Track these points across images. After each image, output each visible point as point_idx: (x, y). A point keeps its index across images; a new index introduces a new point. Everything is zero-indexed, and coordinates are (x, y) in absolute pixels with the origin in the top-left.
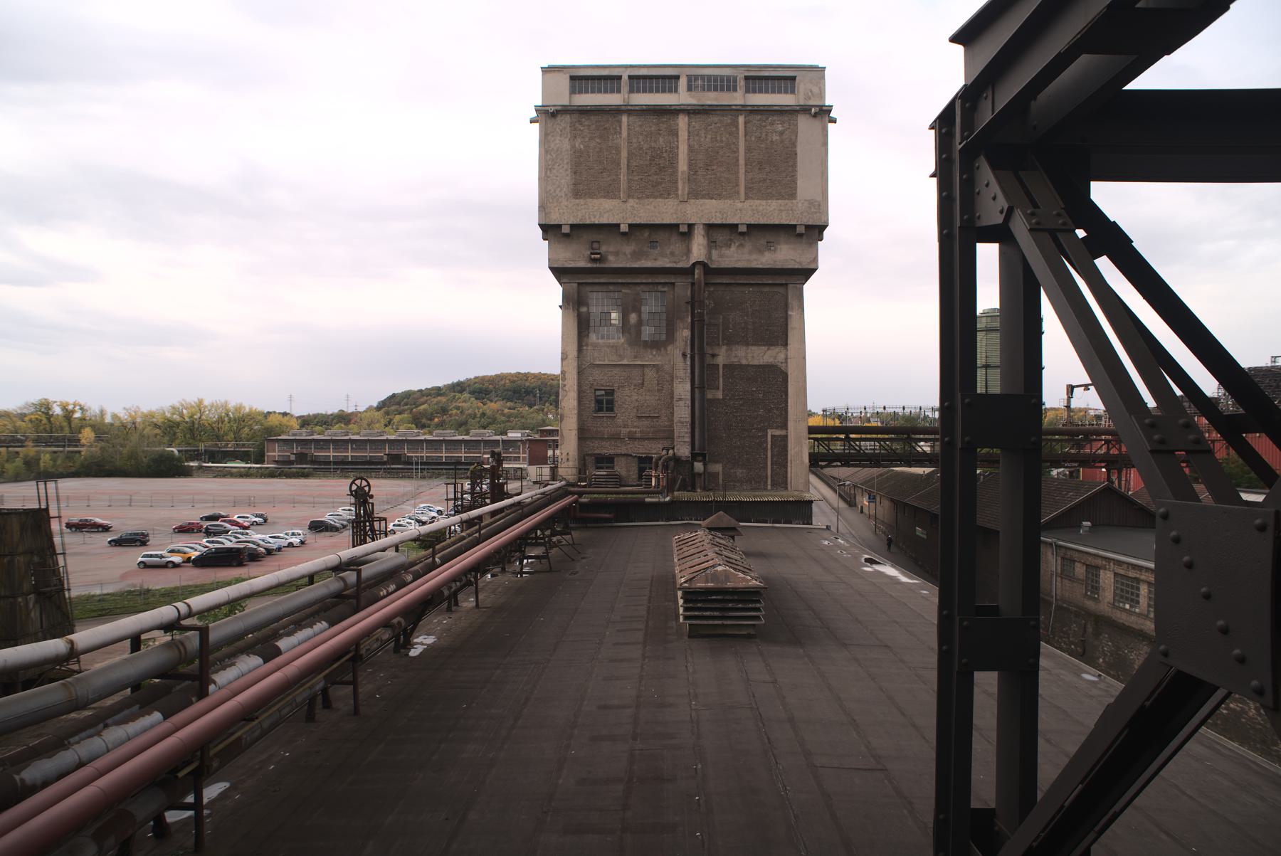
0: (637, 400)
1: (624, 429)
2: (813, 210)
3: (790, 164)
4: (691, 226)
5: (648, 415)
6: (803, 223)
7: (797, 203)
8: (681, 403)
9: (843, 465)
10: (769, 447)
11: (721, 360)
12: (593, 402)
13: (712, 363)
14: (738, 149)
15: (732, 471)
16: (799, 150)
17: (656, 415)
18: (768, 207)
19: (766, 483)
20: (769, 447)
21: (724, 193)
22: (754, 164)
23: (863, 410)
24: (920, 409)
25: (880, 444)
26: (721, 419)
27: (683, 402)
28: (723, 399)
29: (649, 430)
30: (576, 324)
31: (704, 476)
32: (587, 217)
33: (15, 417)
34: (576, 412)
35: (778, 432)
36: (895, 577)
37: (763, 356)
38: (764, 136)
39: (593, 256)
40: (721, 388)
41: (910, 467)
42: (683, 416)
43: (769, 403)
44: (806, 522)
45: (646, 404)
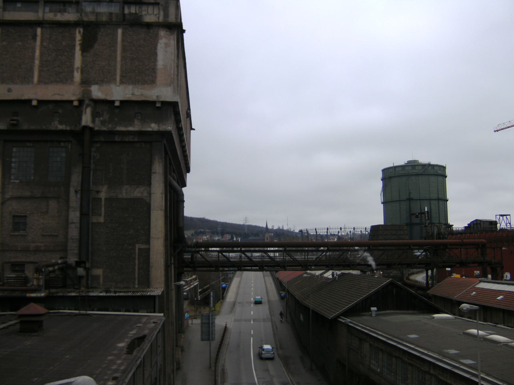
5: (49, 234)
8: (73, 226)
10: (137, 257)
11: (103, 195)
17: (56, 234)
20: (137, 257)
21: (106, 80)
23: (339, 230)
31: (87, 280)
35: (143, 246)
36: (437, 361)
39: (11, 122)
40: (103, 214)
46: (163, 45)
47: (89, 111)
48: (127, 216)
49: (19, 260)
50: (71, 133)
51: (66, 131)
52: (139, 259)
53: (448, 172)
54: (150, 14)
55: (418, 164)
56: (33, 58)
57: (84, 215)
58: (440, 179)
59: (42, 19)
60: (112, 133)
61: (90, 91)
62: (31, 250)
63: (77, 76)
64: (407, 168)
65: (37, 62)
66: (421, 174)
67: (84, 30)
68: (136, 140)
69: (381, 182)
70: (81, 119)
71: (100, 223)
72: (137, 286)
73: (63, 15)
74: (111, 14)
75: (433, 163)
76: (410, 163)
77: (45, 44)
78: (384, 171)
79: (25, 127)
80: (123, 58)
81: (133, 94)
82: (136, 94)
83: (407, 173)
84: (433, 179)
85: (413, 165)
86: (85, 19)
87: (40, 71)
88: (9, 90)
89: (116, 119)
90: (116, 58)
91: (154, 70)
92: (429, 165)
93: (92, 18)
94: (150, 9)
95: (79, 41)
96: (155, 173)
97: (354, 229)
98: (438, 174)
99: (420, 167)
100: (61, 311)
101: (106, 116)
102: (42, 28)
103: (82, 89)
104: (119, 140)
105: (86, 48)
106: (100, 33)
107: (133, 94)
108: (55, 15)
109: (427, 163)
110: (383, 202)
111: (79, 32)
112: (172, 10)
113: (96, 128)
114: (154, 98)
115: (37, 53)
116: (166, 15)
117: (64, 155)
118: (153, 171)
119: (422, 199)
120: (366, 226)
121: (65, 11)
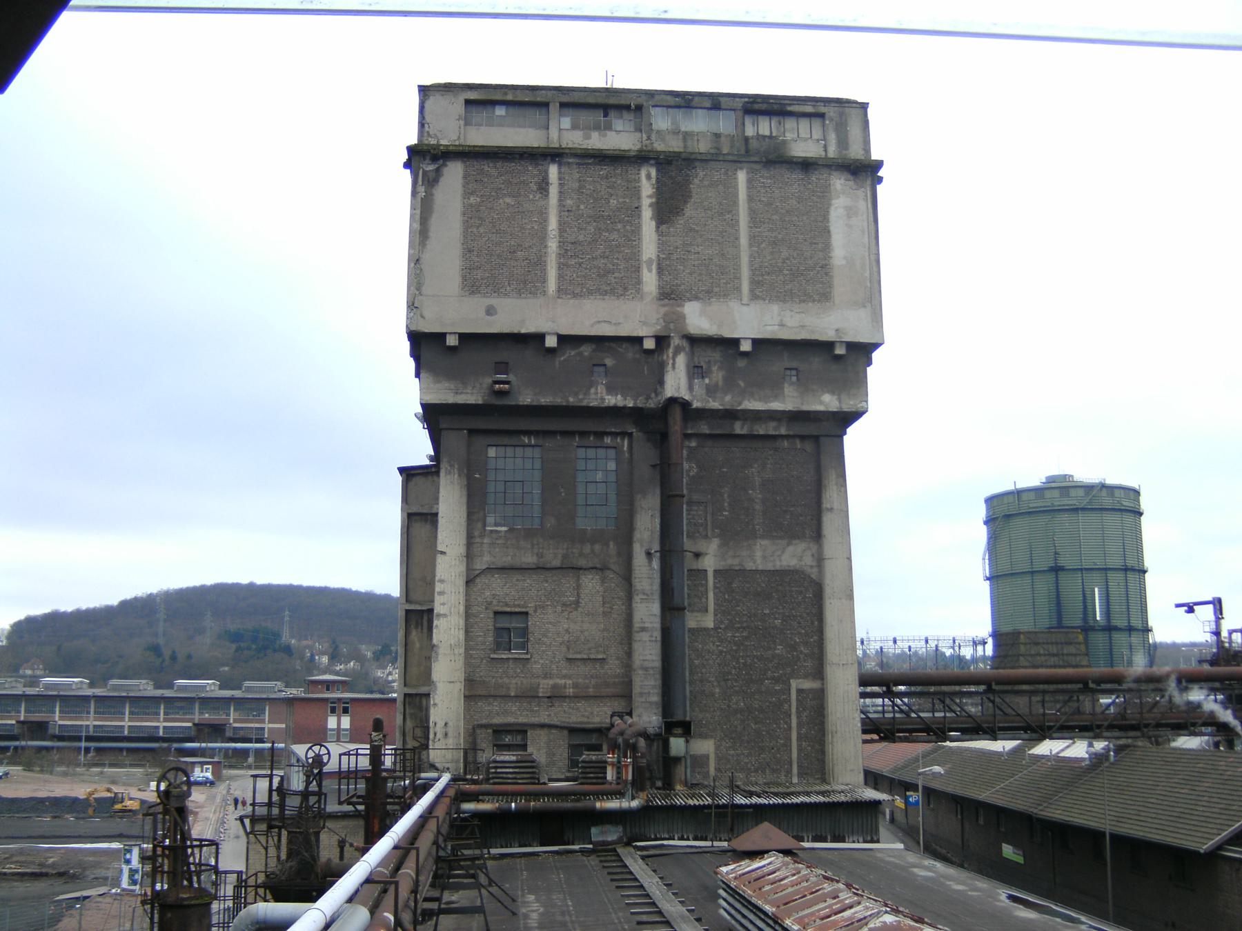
0: (567, 631)
1: (546, 681)
5: (585, 657)
8: (645, 636)
9: (882, 739)
10: (794, 710)
11: (709, 563)
12: (491, 634)
13: (695, 567)
17: (600, 656)
20: (794, 710)
21: (716, 290)
22: (763, 245)
24: (954, 641)
25: (893, 702)
26: (711, 662)
27: (649, 634)
28: (716, 628)
29: (587, 681)
30: (464, 500)
33: (1188, 680)
34: (462, 650)
35: (808, 684)
37: (780, 556)
41: (995, 739)
42: (649, 657)
43: (792, 634)
44: (869, 838)
45: (582, 637)
46: (841, 211)
47: (681, 360)
48: (767, 611)
49: (511, 720)
50: (637, 415)
51: (624, 408)
52: (798, 713)
53: (1145, 503)
54: (806, 140)
55: (1073, 484)
56: (543, 237)
57: (671, 607)
58: (1128, 518)
59: (557, 146)
60: (730, 415)
61: (682, 317)
62: (541, 695)
63: (650, 280)
64: (1048, 494)
65: (553, 245)
66: (1083, 509)
67: (658, 171)
68: (783, 431)
69: (984, 529)
70: (661, 382)
71: (706, 629)
72: (795, 780)
73: (605, 136)
74: (717, 136)
75: (1111, 480)
76: (1054, 482)
77: (569, 202)
78: (991, 501)
79: (526, 398)
80: (753, 239)
81: (782, 325)
82: (789, 324)
83: (1049, 506)
84: (1111, 519)
85: (1060, 486)
86: (659, 146)
87: (561, 267)
88: (490, 311)
89: (742, 384)
90: (737, 239)
91: (825, 268)
92: (1103, 486)
93: (675, 145)
94: (804, 124)
95: (650, 197)
96: (831, 509)
97: (895, 641)
98: (1123, 508)
99: (1081, 492)
100: (665, 842)
101: (718, 375)
102: (560, 165)
103: (663, 310)
104: (744, 431)
105: (666, 212)
106: (696, 181)
107: (782, 325)
108: (588, 137)
109: (1097, 481)
110: (988, 575)
111: (649, 177)
112: (854, 131)
113: (696, 405)
114: (829, 336)
115: (553, 224)
116: (843, 143)
117: (612, 466)
118: (826, 505)
119: (1086, 569)
120: (926, 635)
121: (609, 127)
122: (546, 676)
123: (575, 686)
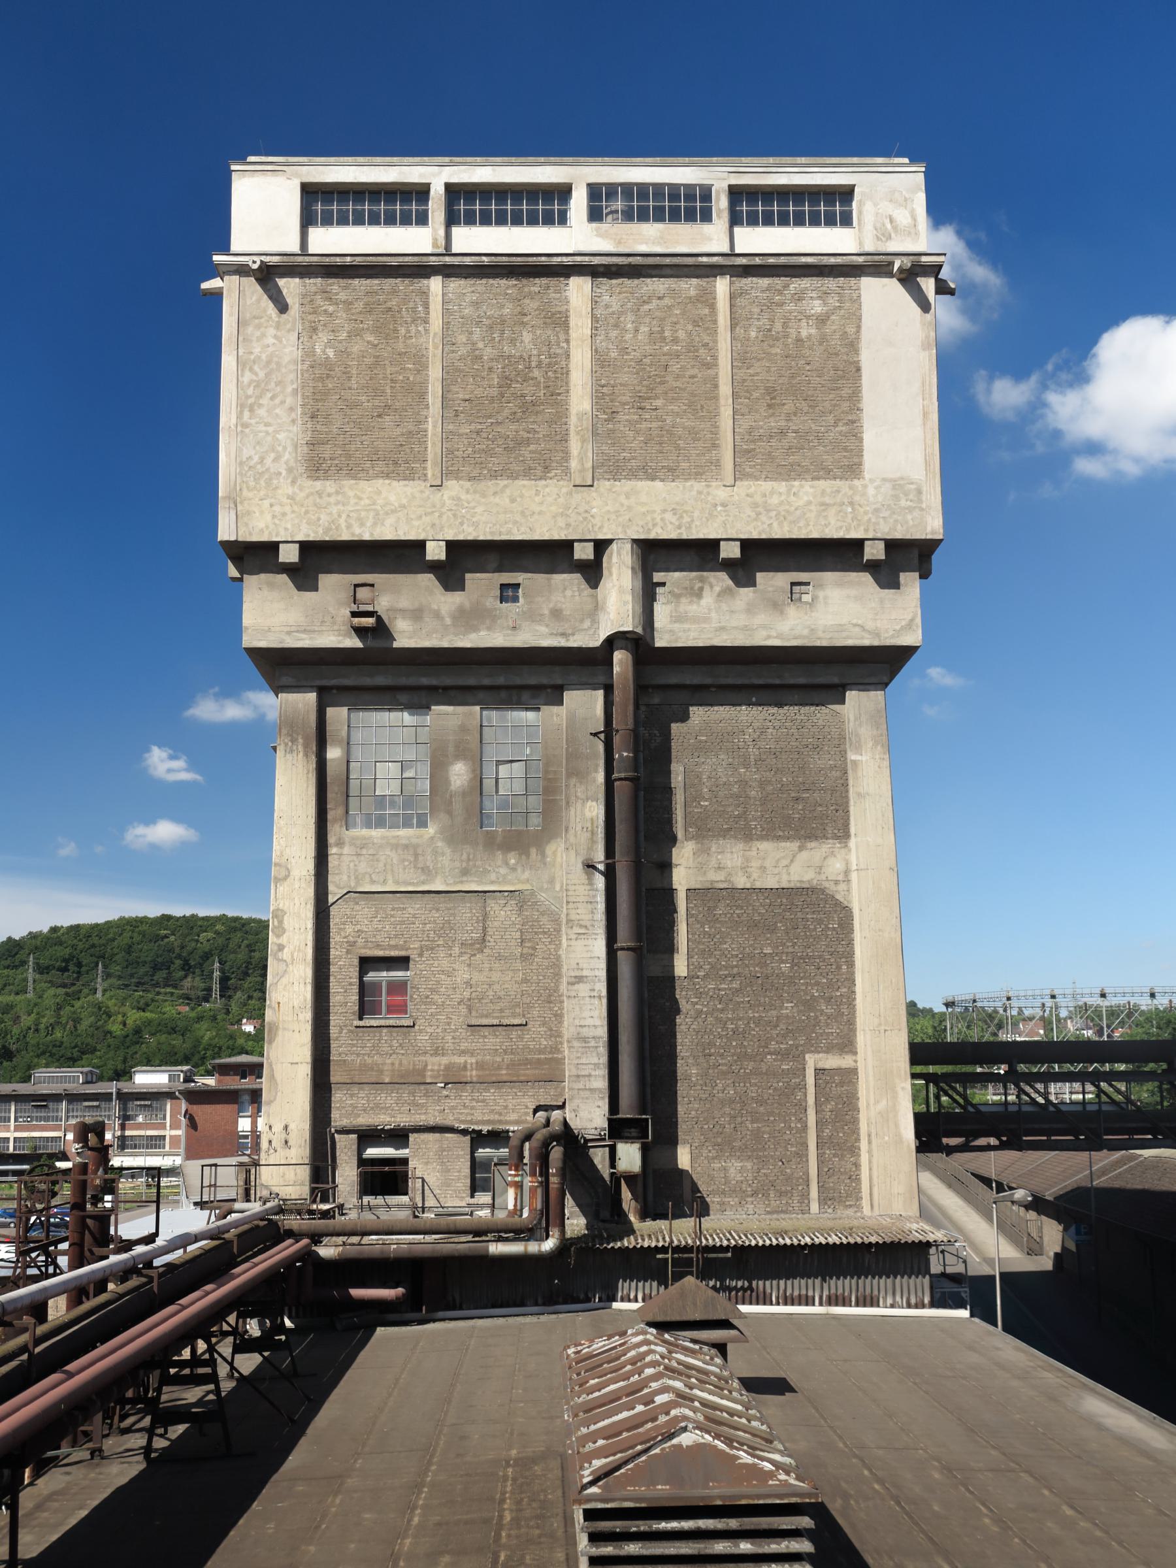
0: (468, 984)
2: (903, 503)
3: (846, 392)
4: (601, 546)
5: (496, 1022)
6: (879, 535)
7: (865, 486)
14: (715, 358)
15: (717, 1165)
16: (866, 358)
18: (792, 498)
19: (805, 1196)
32: (343, 525)
35: (832, 1061)
38: (778, 326)
48: (768, 950)
122: (438, 1051)
123: (480, 1066)
